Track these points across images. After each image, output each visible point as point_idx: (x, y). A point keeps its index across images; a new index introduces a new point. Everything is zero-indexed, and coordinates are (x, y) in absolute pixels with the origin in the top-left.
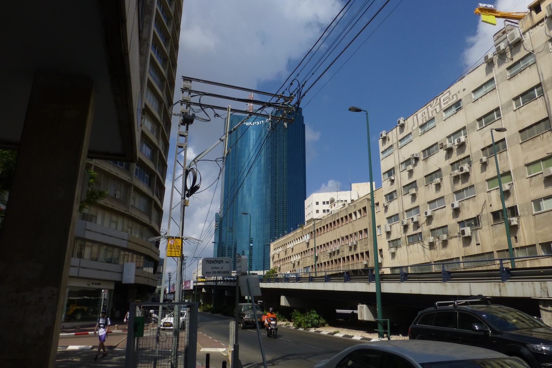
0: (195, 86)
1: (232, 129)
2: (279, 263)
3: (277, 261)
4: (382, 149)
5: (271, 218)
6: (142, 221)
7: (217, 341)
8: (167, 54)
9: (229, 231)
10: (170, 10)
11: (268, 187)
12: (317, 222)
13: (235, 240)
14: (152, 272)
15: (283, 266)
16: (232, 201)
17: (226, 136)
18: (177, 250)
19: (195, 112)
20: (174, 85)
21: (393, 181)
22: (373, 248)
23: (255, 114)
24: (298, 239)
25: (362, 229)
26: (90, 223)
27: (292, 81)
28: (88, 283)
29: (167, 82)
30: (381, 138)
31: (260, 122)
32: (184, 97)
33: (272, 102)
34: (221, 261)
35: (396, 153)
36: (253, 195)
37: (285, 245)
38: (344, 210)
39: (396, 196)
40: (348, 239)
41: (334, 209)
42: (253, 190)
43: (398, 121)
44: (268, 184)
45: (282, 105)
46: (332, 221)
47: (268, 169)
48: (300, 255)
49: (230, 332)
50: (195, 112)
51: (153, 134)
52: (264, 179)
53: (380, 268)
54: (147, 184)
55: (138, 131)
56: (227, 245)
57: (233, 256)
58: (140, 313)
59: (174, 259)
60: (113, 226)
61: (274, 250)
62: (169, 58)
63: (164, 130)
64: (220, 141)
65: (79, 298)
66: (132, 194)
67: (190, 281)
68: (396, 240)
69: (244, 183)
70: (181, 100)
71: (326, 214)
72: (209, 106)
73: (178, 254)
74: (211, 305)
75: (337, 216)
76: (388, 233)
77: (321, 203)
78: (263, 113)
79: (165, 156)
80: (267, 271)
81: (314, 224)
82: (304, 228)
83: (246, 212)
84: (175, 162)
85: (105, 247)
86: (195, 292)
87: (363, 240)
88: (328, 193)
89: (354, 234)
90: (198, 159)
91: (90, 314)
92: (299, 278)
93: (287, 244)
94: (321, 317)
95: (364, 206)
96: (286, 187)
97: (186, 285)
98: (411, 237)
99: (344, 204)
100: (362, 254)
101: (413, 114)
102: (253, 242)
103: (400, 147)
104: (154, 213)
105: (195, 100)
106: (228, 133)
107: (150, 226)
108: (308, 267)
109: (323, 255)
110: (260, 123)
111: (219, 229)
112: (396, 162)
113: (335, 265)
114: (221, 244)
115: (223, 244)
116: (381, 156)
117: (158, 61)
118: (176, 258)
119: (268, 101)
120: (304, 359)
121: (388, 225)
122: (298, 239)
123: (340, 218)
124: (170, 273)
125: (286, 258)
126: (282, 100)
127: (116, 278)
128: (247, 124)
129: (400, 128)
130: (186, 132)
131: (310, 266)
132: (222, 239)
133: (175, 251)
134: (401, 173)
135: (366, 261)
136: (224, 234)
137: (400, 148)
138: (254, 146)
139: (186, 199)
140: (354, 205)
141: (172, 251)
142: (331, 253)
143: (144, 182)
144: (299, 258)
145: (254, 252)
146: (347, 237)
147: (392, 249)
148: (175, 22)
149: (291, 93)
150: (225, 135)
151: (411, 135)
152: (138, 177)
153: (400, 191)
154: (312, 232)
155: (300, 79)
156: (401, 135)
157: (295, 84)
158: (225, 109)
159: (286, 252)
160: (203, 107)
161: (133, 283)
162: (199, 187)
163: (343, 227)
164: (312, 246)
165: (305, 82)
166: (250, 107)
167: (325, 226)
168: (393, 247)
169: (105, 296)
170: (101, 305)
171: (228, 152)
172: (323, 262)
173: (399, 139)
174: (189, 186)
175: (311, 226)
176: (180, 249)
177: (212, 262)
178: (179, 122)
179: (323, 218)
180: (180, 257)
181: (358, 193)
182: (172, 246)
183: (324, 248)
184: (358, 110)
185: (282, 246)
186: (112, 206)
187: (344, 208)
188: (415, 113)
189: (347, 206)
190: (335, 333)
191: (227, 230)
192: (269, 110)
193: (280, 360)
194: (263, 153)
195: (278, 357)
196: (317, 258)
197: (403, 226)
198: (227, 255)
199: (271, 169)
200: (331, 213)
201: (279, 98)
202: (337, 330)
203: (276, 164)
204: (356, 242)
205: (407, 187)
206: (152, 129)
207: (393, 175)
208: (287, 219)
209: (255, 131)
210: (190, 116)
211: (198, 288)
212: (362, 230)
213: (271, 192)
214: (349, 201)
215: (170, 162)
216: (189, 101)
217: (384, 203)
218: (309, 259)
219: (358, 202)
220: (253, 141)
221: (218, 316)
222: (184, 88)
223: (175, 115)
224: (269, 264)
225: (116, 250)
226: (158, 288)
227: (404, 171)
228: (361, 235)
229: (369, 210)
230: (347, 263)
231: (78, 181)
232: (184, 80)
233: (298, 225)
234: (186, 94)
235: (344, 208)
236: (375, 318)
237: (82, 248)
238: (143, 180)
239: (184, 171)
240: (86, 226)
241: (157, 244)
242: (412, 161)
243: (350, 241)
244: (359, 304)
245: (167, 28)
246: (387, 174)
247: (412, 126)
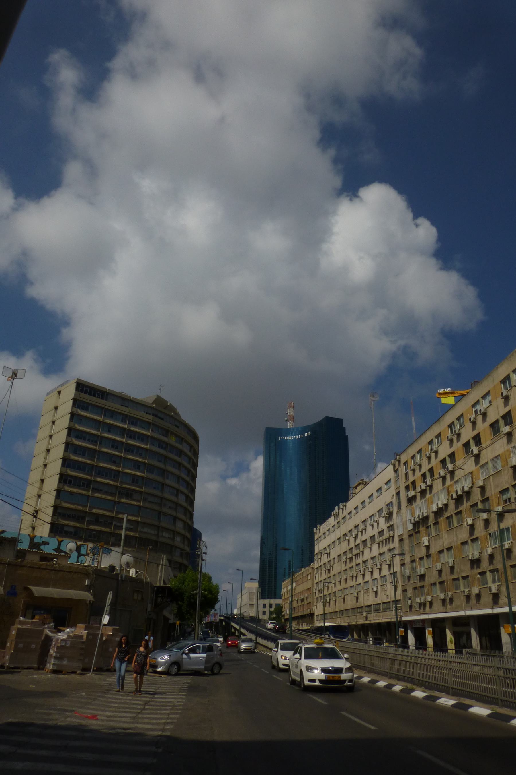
31: (300, 436)
123: (322, 563)
128: (286, 438)
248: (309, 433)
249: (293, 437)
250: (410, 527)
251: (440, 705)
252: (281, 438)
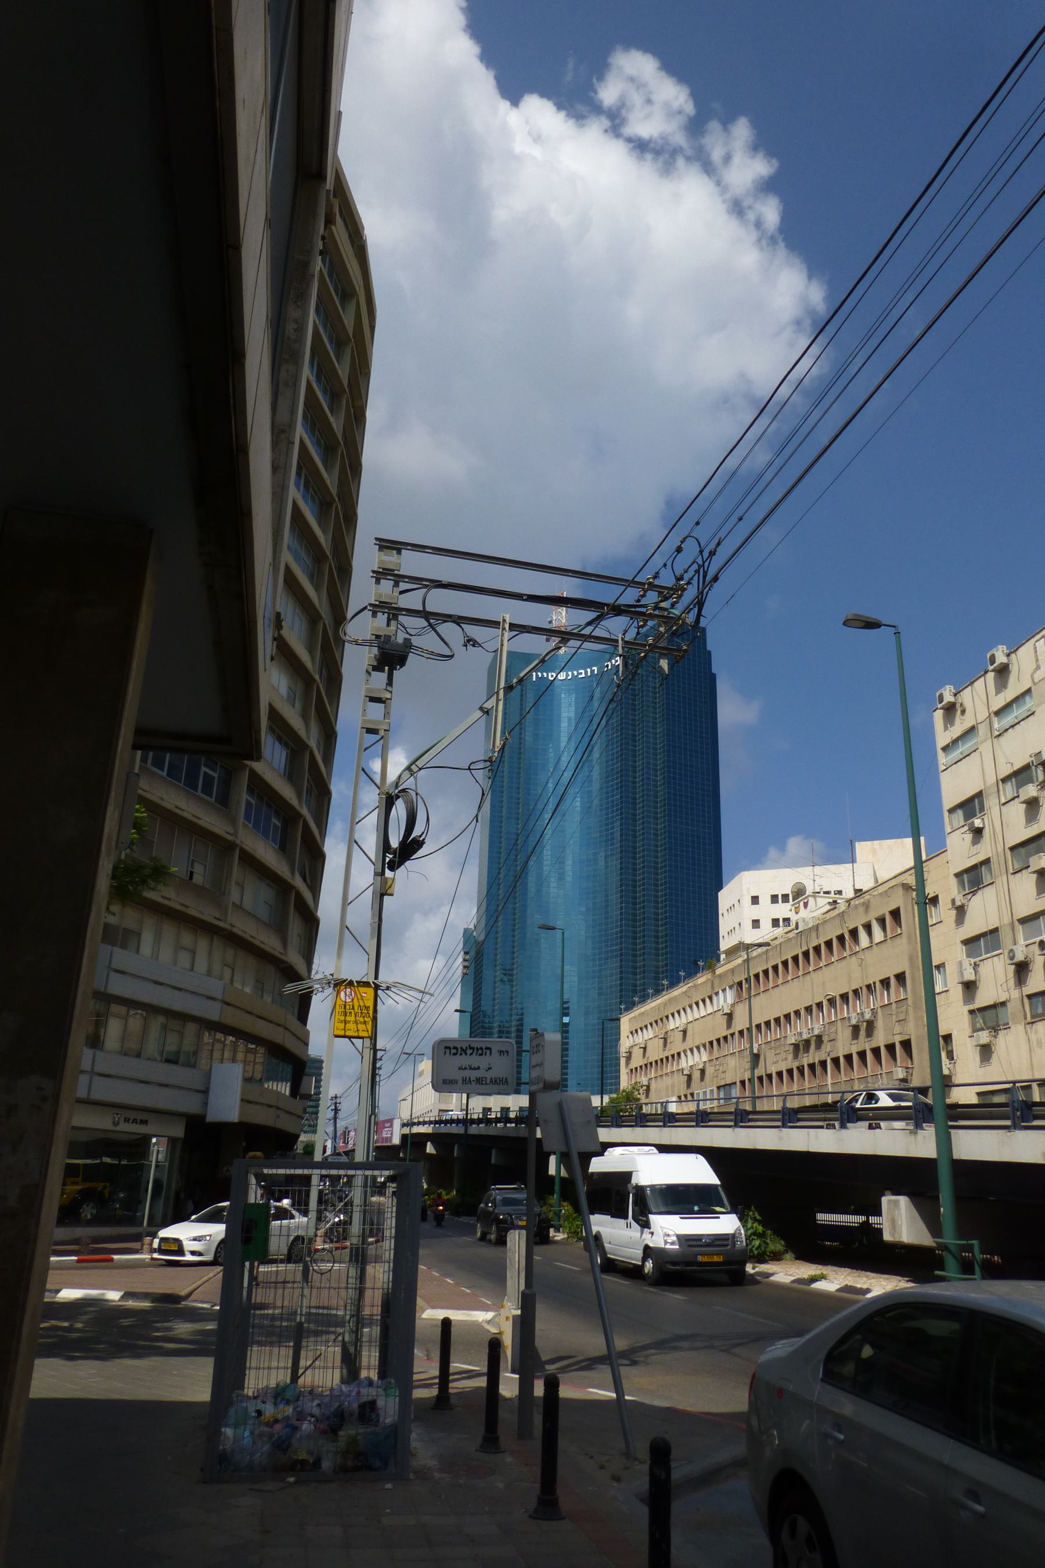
0: (410, 563)
1: (515, 681)
2: (646, 1074)
3: (641, 1067)
4: (943, 738)
5: (621, 943)
6: (262, 946)
7: (468, 1291)
8: (331, 489)
9: (502, 981)
10: (340, 371)
11: (612, 855)
12: (755, 954)
13: (519, 1006)
14: (288, 1093)
15: (656, 1081)
16: (511, 890)
17: (498, 700)
18: (362, 1019)
19: (410, 635)
20: (351, 572)
21: (978, 832)
22: (924, 1031)
23: (578, 636)
24: (701, 1004)
25: (890, 973)
26: (120, 950)
27: (682, 542)
28: (115, 1118)
29: (330, 564)
30: (940, 706)
31: (589, 670)
32: (381, 595)
33: (621, 601)
34: (487, 1048)
35: (986, 748)
36: (569, 879)
37: (661, 1019)
38: (834, 917)
39: (989, 876)
40: (847, 1004)
41: (803, 916)
42: (569, 862)
43: (990, 657)
44: (612, 844)
45: (654, 610)
46: (799, 952)
47: (613, 801)
48: (705, 1049)
49: (508, 1261)
50: (410, 635)
51: (294, 706)
52: (600, 832)
53: (947, 1086)
54: (276, 844)
55: (265, 670)
56: (496, 1019)
57: (513, 1035)
58: (260, 1192)
59: (353, 1044)
60: (184, 958)
61: (630, 1036)
62: (337, 499)
63: (324, 694)
64: (479, 714)
65: (89, 1161)
66: (236, 871)
67: (391, 1121)
68: (994, 1006)
69: (545, 841)
70: (373, 602)
71: (780, 931)
72: (450, 616)
73: (365, 1030)
74: (451, 1191)
75: (814, 935)
76: (970, 987)
77: (765, 899)
78: (598, 632)
79: (326, 766)
80: (612, 1096)
81: (747, 961)
82: (719, 971)
83: (551, 924)
84: (357, 771)
85: (161, 1019)
86: (405, 1154)
87: (894, 1005)
88: (787, 871)
89: (865, 989)
90: (420, 763)
91: (118, 1206)
92: (744, 1114)
93: (667, 1017)
94: (769, 1232)
95: (893, 907)
96: (665, 855)
97: (382, 1132)
98: (1040, 999)
99: (835, 902)
100: (891, 1048)
101: (1033, 637)
102: (571, 1011)
103: (998, 733)
104: (295, 927)
105: (412, 600)
106: (501, 692)
107: (284, 962)
108: (730, 1085)
109: (773, 1051)
110: (589, 674)
111: (475, 967)
112: (987, 778)
113: (809, 1082)
114: (479, 1017)
115: (484, 1016)
116: (942, 759)
117: (307, 509)
118: (358, 1042)
119: (611, 601)
120: (723, 1351)
121: (967, 963)
122: (701, 1004)
123: (822, 941)
124: (336, 1097)
125: (667, 1058)
126: (652, 597)
127: (189, 1104)
128: (552, 676)
129: (944, 713)
130: (386, 690)
131: (735, 1083)
132: (483, 1002)
133: (356, 1022)
134: (1002, 807)
135: (904, 1071)
136: (487, 990)
137: (999, 735)
138: (569, 739)
139: (386, 876)
140: (863, 904)
141: (349, 1022)
142: (799, 1045)
143: (268, 840)
144: (705, 1057)
145: (574, 1042)
146: (844, 997)
147: (980, 1033)
148: (352, 402)
149: (678, 574)
150: (495, 697)
151: (1031, 697)
152: (251, 826)
153: (1002, 862)
154: (740, 984)
155: (703, 533)
156: (1001, 696)
157: (691, 550)
158: (494, 624)
159: (665, 1039)
160: (432, 621)
161: (236, 1120)
162: (423, 842)
163: (832, 967)
164: (741, 1022)
165: (719, 544)
166: (561, 617)
167: (780, 967)
168: (982, 1029)
169: (160, 1156)
170: (148, 1182)
171: (504, 744)
172: (773, 1070)
173: (995, 707)
174: (394, 843)
175: (739, 965)
176: (371, 1016)
177: (460, 1050)
178: (367, 663)
179: (774, 942)
180: (371, 1040)
181: (876, 869)
182: (348, 1007)
183: (776, 1030)
184: (871, 625)
185: (654, 1024)
186: (181, 904)
187: (836, 912)
188: (1041, 631)
189: (842, 906)
190: (814, 1279)
191: (495, 977)
192: (615, 626)
193: (653, 1351)
194: (596, 754)
195: (647, 1342)
196: (756, 1058)
197: (1014, 966)
198: (496, 1030)
199: (622, 803)
200: (797, 927)
201: (643, 589)
202: (818, 1272)
203: (634, 788)
204: (873, 1013)
205: (1022, 850)
206: (291, 692)
207: (979, 815)
208: (666, 911)
209: (574, 696)
210: (398, 644)
211: (413, 1142)
212: (889, 978)
213: (621, 869)
214: (849, 894)
215: (339, 788)
216: (393, 605)
217: (953, 897)
218: (734, 1061)
219: (876, 893)
220: (569, 724)
221: (472, 1222)
222: (381, 570)
223: (356, 642)
224: (618, 1077)
225: (191, 1028)
226: (302, 1142)
227: (1012, 802)
228: (886, 992)
229: (910, 917)
230: (845, 1075)
231: (113, 794)
232: (381, 548)
233: (701, 963)
234: (387, 585)
235: (836, 912)
236: (934, 1237)
237: (100, 1021)
238: (266, 835)
239: (381, 798)
240: (110, 962)
241: (304, 1002)
242: (1036, 772)
243: (855, 1010)
244: (884, 1195)
245: (332, 419)
246: (960, 813)
247: (1031, 671)
248: (617, 661)
249: (570, 673)
251: (907, 1293)
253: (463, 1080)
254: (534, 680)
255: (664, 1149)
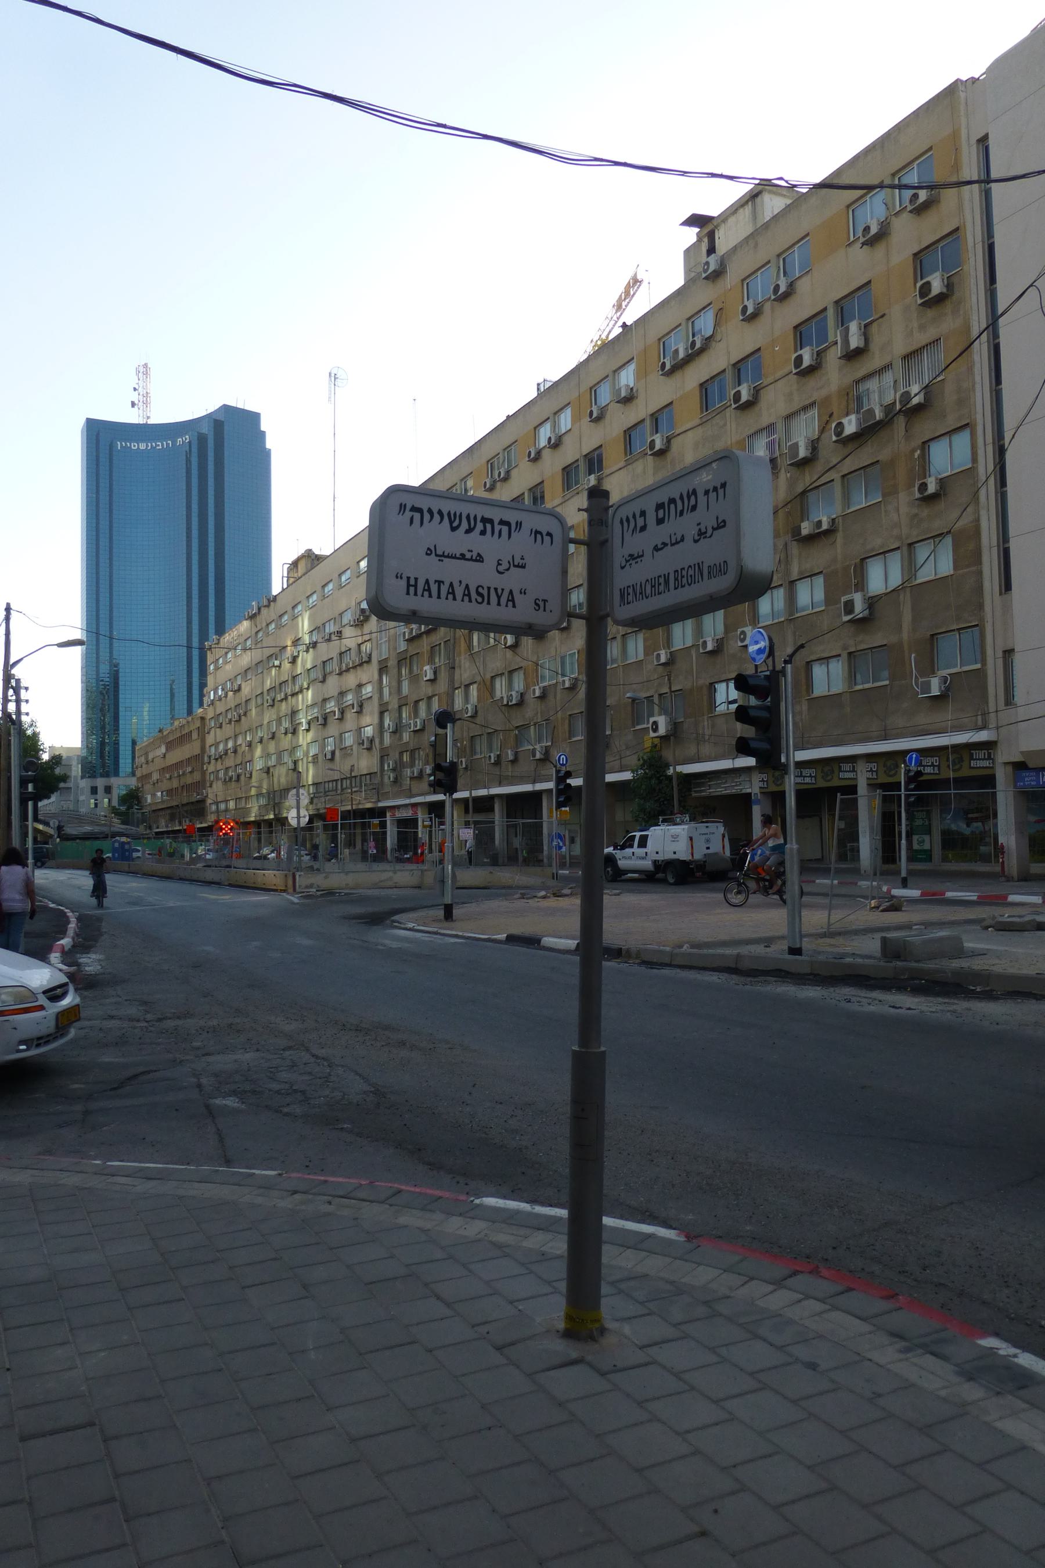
31: (165, 443)
34: (502, 522)
128: (134, 446)
190: (1015, 1356)
248: (186, 439)
249: (149, 444)
250: (403, 646)
252: (121, 444)
253: (409, 585)
254: (119, 448)
255: (1007, 585)
